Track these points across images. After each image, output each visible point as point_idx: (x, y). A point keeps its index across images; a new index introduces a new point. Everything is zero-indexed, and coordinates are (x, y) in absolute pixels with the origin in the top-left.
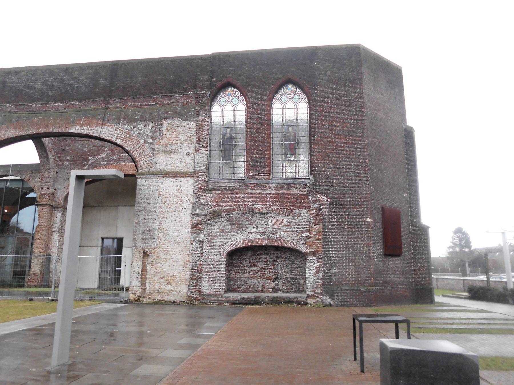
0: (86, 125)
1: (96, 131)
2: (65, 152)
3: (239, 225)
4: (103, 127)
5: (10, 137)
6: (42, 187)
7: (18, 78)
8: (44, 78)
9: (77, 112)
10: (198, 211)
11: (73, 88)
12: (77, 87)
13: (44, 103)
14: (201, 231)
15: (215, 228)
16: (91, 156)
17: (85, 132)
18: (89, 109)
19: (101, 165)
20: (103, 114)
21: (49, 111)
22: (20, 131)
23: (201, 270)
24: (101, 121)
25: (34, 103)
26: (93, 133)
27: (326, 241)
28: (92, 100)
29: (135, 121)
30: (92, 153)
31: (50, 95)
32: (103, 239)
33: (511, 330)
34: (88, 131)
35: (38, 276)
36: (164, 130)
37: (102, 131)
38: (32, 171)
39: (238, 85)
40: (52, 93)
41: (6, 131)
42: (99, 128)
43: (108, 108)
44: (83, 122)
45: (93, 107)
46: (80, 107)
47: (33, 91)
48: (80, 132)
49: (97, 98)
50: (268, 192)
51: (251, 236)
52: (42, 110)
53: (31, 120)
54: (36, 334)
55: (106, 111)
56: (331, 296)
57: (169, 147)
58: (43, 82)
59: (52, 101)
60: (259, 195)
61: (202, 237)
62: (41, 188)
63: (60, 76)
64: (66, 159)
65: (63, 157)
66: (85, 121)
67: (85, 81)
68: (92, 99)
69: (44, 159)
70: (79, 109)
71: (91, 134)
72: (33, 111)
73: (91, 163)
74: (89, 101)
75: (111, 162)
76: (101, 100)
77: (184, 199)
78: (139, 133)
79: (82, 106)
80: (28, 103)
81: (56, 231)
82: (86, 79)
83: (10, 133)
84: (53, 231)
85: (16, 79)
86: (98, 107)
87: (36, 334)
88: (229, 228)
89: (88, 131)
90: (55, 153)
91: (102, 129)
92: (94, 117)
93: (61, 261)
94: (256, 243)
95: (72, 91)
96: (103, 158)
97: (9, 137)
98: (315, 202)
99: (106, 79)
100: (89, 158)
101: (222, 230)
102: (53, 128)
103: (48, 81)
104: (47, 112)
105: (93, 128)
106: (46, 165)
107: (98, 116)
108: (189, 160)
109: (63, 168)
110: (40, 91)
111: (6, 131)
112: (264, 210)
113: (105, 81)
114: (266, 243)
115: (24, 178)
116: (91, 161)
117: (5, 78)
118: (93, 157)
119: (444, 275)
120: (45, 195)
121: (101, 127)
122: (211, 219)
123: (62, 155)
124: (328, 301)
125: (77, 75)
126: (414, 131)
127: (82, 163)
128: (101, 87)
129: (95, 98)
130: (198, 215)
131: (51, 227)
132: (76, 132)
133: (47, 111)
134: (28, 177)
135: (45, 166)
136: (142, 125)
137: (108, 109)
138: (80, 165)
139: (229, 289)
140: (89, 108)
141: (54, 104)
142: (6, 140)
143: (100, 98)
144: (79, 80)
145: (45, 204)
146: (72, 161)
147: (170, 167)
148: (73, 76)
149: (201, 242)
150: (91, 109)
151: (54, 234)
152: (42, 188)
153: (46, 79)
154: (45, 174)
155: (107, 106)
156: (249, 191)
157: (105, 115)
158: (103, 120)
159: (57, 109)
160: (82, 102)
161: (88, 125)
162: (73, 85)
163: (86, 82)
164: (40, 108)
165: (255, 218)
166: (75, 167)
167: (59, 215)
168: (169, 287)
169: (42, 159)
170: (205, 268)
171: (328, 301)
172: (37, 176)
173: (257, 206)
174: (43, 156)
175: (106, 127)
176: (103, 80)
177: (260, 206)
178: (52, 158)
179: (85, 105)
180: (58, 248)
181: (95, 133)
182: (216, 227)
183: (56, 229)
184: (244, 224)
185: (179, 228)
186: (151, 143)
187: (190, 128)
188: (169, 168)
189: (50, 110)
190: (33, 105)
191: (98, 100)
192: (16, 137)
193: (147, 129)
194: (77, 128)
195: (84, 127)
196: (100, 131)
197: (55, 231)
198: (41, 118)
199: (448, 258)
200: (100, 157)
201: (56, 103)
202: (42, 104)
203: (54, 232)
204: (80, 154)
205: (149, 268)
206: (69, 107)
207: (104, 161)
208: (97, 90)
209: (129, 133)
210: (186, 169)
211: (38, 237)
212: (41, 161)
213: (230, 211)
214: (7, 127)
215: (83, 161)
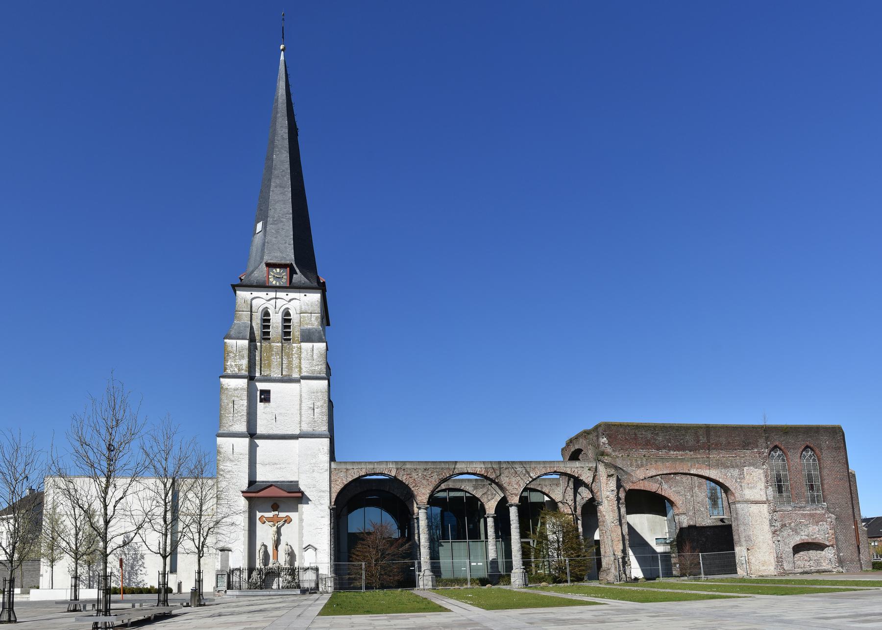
3: (796, 531)
23: (782, 557)
27: (836, 538)
29: (728, 467)
33: (879, 582)
36: (745, 473)
39: (783, 447)
42: (708, 471)
50: (805, 512)
51: (803, 537)
56: (842, 567)
57: (750, 485)
60: (802, 514)
61: (779, 538)
71: (704, 474)
77: (764, 517)
78: (732, 475)
88: (792, 533)
92: (704, 463)
94: (805, 541)
98: (828, 518)
101: (789, 534)
108: (763, 493)
114: (810, 541)
119: (459, 620)
122: (782, 528)
124: (841, 570)
126: (280, 544)
136: (732, 470)
147: (753, 497)
156: (797, 512)
164: (664, 454)
165: (803, 527)
168: (764, 568)
170: (784, 556)
171: (841, 570)
173: (802, 520)
177: (803, 521)
181: (706, 474)
182: (785, 533)
184: (798, 531)
185: (763, 534)
186: (740, 482)
187: (759, 473)
188: (752, 498)
193: (736, 472)
209: (725, 475)
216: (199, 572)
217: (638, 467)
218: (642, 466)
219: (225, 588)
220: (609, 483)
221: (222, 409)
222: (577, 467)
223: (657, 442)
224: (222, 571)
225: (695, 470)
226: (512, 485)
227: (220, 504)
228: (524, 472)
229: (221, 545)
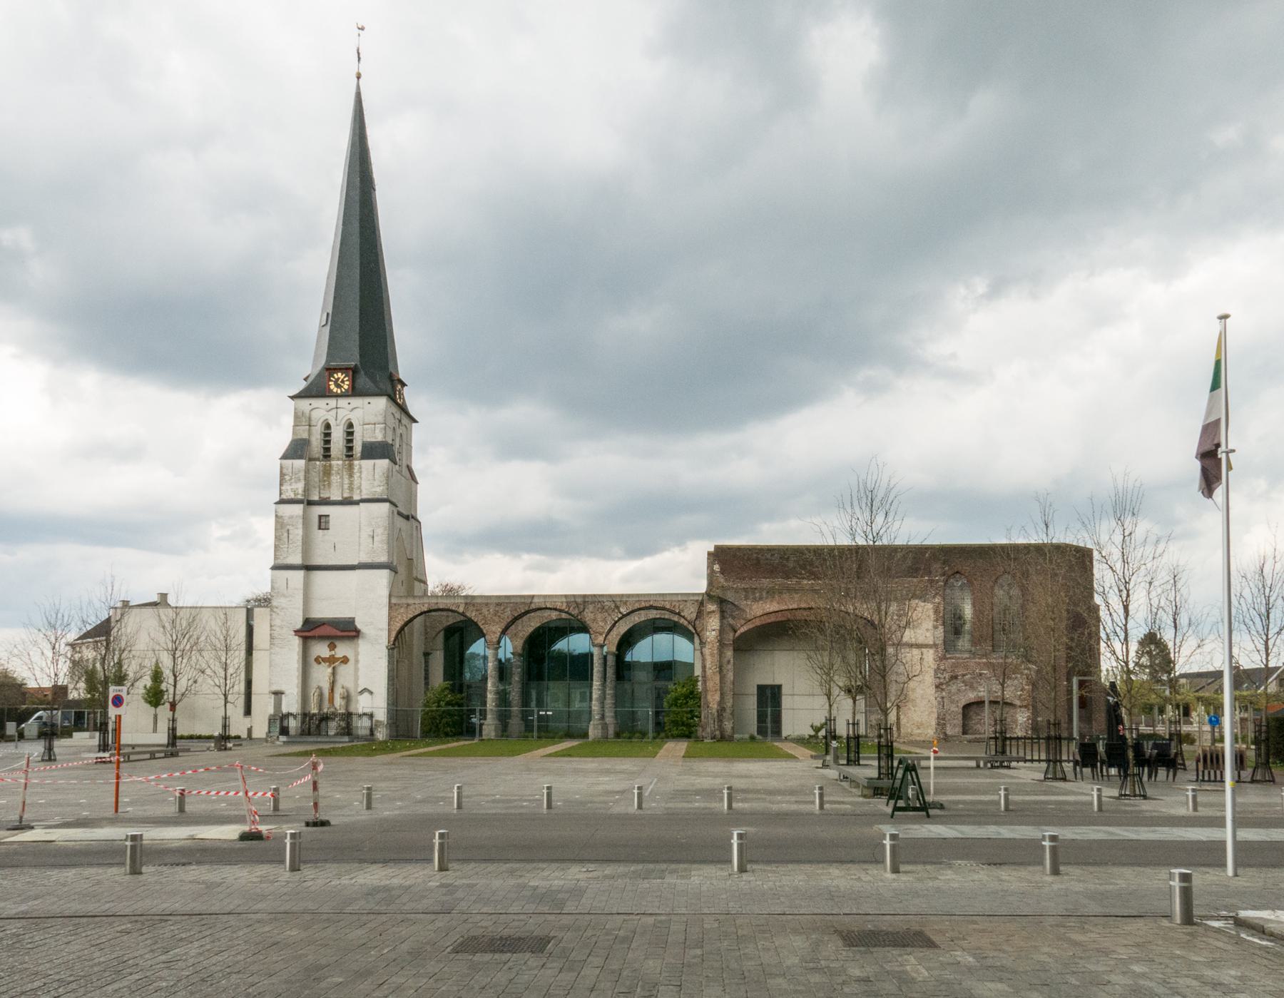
10: (939, 675)
14: (943, 690)
15: (954, 688)
54: (321, 695)
85: (769, 556)
87: (321, 695)
112: (988, 675)
130: (939, 678)
139: (964, 733)
149: (943, 698)
168: (919, 731)
170: (948, 717)
199: (1213, 483)
205: (902, 717)
210: (926, 642)
213: (964, 675)
214: (772, 601)
218: (761, 599)
219: (277, 734)
224: (274, 715)
227: (274, 644)
229: (275, 688)
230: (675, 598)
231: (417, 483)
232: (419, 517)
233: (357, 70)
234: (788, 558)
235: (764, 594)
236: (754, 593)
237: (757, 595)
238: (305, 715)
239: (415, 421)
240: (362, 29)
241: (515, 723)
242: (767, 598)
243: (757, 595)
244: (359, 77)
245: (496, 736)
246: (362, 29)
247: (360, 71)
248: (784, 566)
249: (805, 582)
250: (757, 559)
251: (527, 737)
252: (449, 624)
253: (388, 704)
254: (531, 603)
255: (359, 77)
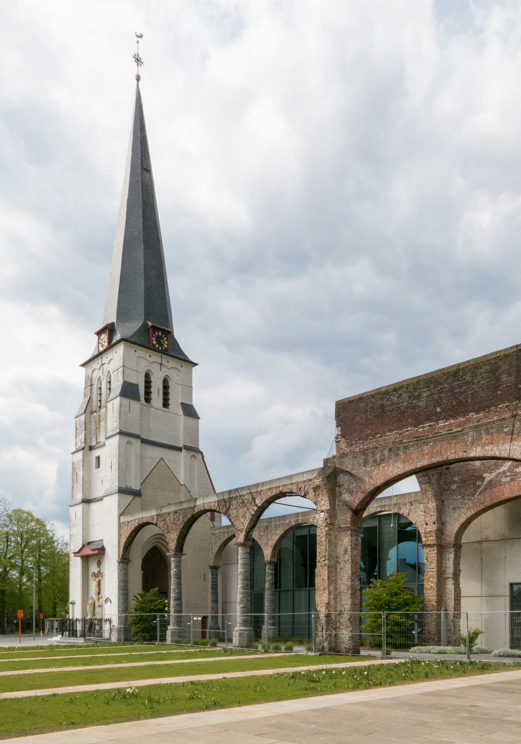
0: (489, 443)
1: (504, 450)
2: (451, 471)
4: (512, 444)
5: (399, 473)
6: (427, 522)
7: (398, 398)
8: (428, 390)
9: (475, 428)
11: (466, 397)
12: (472, 394)
13: (432, 423)
16: (487, 472)
17: (490, 454)
18: (491, 422)
19: (502, 483)
20: (511, 425)
21: (439, 433)
22: (410, 464)
24: (509, 435)
25: (421, 426)
26: (500, 454)
28: (493, 408)
30: (488, 467)
31: (438, 412)
32: (162, 458)
34: (492, 452)
35: (434, 635)
37: (511, 449)
38: (411, 503)
40: (440, 408)
41: (394, 467)
42: (507, 446)
43: (517, 415)
44: (485, 440)
45: (496, 418)
46: (479, 421)
47: (417, 410)
48: (483, 455)
49: (499, 405)
52: (431, 434)
53: (420, 449)
55: (514, 420)
58: (428, 396)
59: (443, 419)
62: (425, 524)
63: (448, 384)
64: (452, 480)
65: (448, 478)
66: (487, 439)
67: (482, 384)
68: (494, 406)
69: (426, 485)
70: (476, 424)
71: (497, 454)
72: (421, 437)
73: (487, 482)
74: (489, 411)
75: (516, 476)
76: (507, 406)
79: (481, 418)
80: (413, 428)
81: (450, 578)
82: (482, 380)
83: (399, 469)
84: (446, 578)
85: (395, 399)
86: (503, 417)
89: (492, 452)
90: (437, 474)
91: (511, 446)
92: (499, 430)
93: (459, 616)
95: (466, 401)
96: (504, 472)
97: (397, 474)
99: (510, 375)
100: (484, 475)
102: (447, 455)
103: (433, 394)
104: (438, 434)
105: (499, 447)
106: (429, 493)
107: (505, 429)
109: (450, 493)
110: (425, 408)
111: (394, 467)
113: (508, 378)
115: (403, 513)
116: (487, 479)
117: (383, 400)
118: (490, 473)
120: (432, 533)
121: (509, 443)
123: (447, 476)
125: (470, 377)
127: (474, 483)
128: (504, 388)
129: (497, 405)
131: (443, 573)
132: (477, 456)
133: (437, 433)
134: (407, 511)
135: (427, 495)
137: (517, 417)
138: (472, 486)
140: (491, 420)
141: (444, 423)
142: (395, 477)
143: (504, 403)
144: (473, 384)
145: (433, 544)
146: (460, 483)
148: (465, 379)
150: (494, 421)
151: (447, 581)
152: (427, 524)
153: (431, 392)
154: (429, 505)
155: (515, 412)
157: (513, 426)
158: (512, 433)
159: (449, 429)
160: (480, 414)
161: (492, 443)
162: (465, 392)
163: (483, 384)
164: (428, 431)
166: (465, 490)
167: (452, 556)
169: (423, 486)
172: (418, 508)
174: (424, 482)
175: (516, 442)
176: (506, 377)
178: (435, 483)
179: (486, 417)
180: (455, 600)
181: (503, 452)
183: (449, 576)
189: (441, 431)
190: (419, 428)
191: (503, 406)
192: (406, 472)
194: (478, 450)
195: (487, 448)
196: (508, 449)
197: (448, 578)
198: (432, 444)
200: (499, 471)
201: (447, 421)
202: (430, 426)
203: (447, 580)
204: (470, 471)
206: (464, 423)
207: (506, 477)
208: (499, 392)
211: (429, 587)
212: (422, 489)
215: (476, 480)
216: (467, 620)
217: (377, 464)
218: (382, 460)
220: (319, 499)
221: (487, 410)
222: (304, 481)
223: (417, 410)
225: (479, 449)
226: (238, 519)
228: (250, 500)
230: (301, 479)
231: (199, 418)
232: (201, 448)
233: (137, 73)
234: (420, 395)
235: (386, 453)
236: (374, 454)
237: (378, 456)
238: (84, 620)
239: (195, 364)
240: (141, 36)
241: (267, 629)
242: (389, 458)
243: (378, 456)
244: (138, 79)
245: (119, 640)
246: (141, 36)
247: (139, 74)
248: (414, 407)
249: (441, 424)
250: (382, 406)
251: (180, 642)
252: (225, 539)
253: (119, 611)
254: (195, 507)
255: (138, 79)
